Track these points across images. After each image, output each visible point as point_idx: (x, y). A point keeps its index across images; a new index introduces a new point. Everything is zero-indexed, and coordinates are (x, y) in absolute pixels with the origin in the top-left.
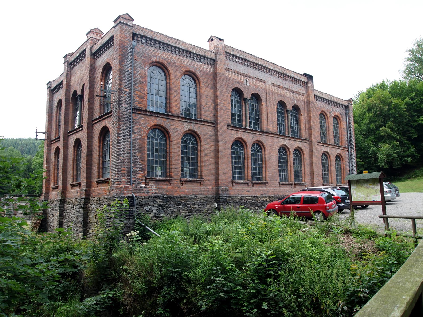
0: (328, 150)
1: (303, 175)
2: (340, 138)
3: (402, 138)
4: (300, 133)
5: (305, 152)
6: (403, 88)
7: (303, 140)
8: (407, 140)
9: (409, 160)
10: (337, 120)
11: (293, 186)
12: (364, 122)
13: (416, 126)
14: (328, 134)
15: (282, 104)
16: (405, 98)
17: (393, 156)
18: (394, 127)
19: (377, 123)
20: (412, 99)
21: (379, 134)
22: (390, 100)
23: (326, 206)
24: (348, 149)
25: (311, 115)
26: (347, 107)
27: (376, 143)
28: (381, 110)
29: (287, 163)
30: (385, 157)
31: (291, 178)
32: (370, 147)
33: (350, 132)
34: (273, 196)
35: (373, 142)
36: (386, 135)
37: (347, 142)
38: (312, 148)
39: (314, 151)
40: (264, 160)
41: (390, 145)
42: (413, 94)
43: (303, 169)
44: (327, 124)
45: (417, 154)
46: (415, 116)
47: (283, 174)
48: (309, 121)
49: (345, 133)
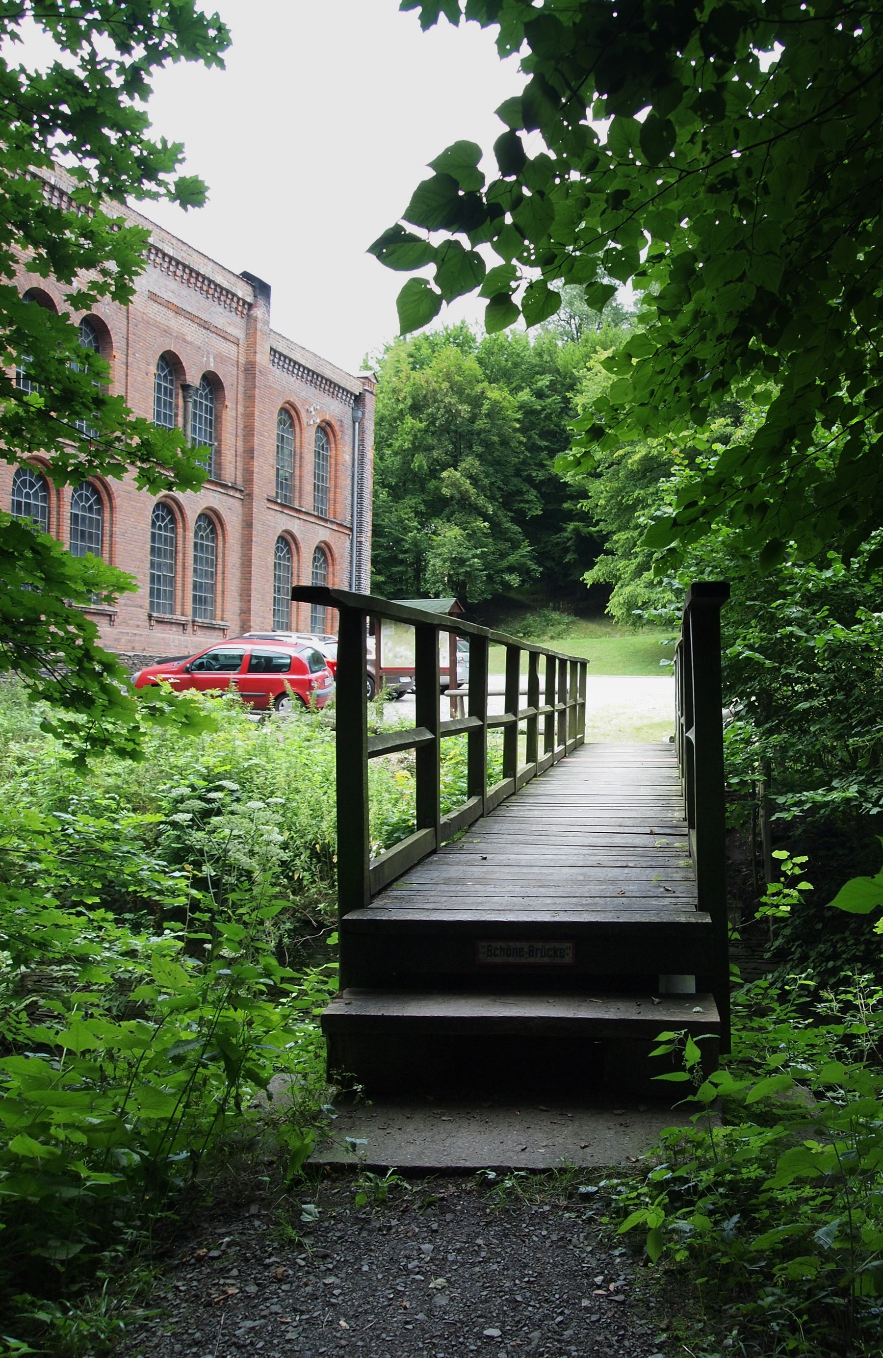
0: (296, 526)
1: (219, 600)
2: (332, 496)
3: (499, 513)
4: (219, 465)
5: (229, 528)
6: (518, 355)
7: (225, 486)
8: (513, 520)
9: (514, 580)
10: (326, 435)
11: (190, 628)
12: (397, 444)
13: (542, 482)
14: (297, 478)
15: (170, 363)
16: (519, 389)
17: (470, 566)
18: (482, 476)
19: (435, 454)
20: (540, 394)
21: (438, 489)
22: (479, 388)
23: (310, 681)
24: (351, 530)
25: (257, 413)
26: (359, 399)
27: (424, 518)
28: (452, 414)
29: (173, 555)
30: (448, 564)
31: (183, 605)
32: (406, 530)
33: (362, 479)
34: (131, 654)
35: (417, 513)
36: (457, 496)
37: (349, 507)
38: (251, 515)
39: (257, 526)
40: (107, 539)
41: (464, 530)
42: (544, 381)
43: (220, 578)
44: (298, 444)
45: (534, 567)
46: (541, 449)
47: (161, 588)
48: (249, 431)
49: (345, 482)
